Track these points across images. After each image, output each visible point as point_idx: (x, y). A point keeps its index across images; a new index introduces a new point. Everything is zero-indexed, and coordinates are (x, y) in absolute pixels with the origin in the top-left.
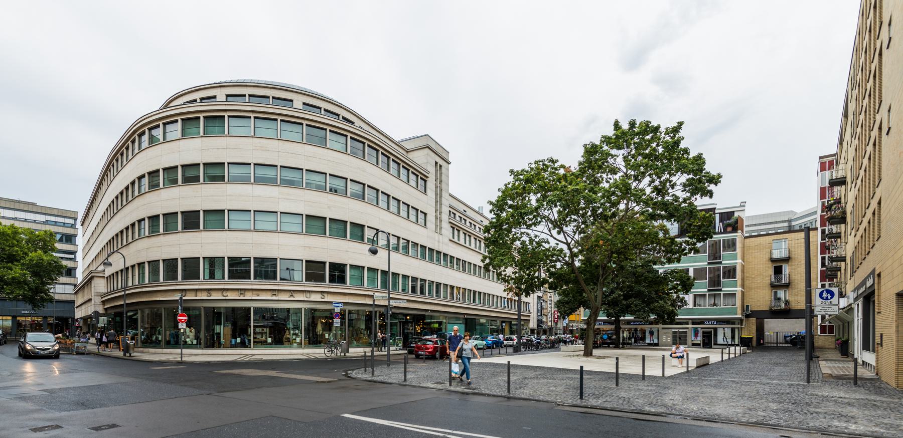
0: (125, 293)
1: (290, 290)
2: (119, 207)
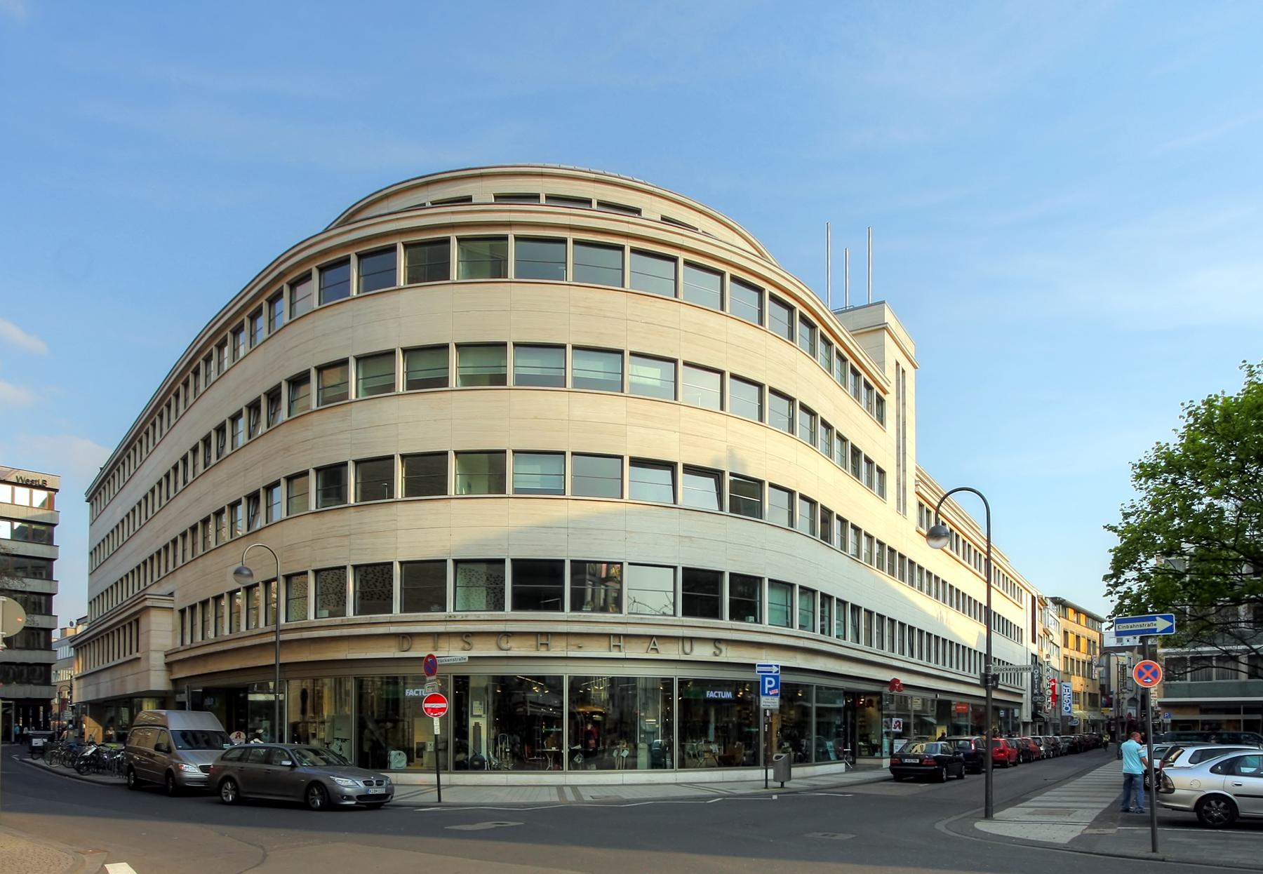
1: (651, 637)
2: (157, 508)
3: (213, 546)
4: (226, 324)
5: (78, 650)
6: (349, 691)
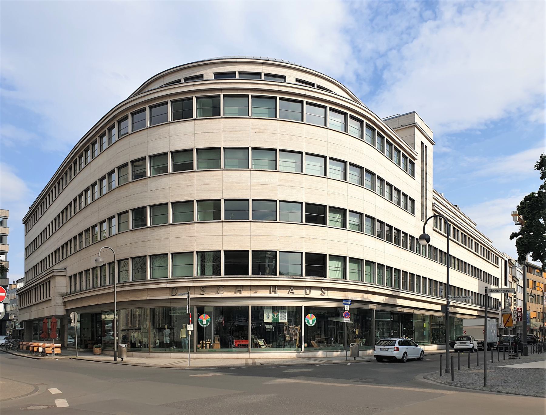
3: (84, 246)
4: (89, 140)
5: (20, 296)
6: (148, 314)
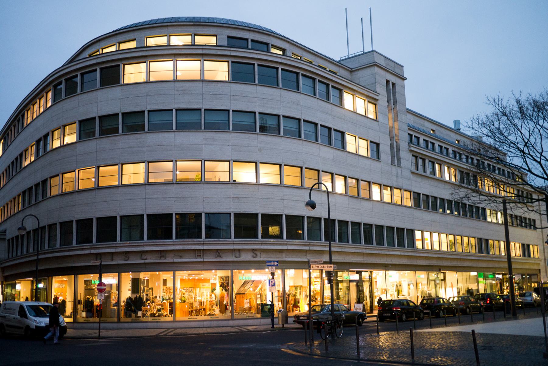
0: (38, 257)
